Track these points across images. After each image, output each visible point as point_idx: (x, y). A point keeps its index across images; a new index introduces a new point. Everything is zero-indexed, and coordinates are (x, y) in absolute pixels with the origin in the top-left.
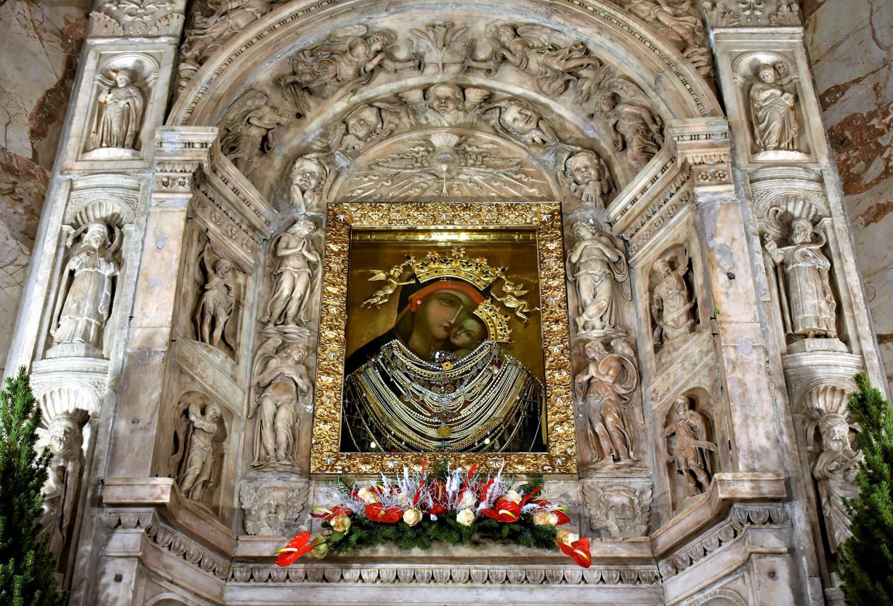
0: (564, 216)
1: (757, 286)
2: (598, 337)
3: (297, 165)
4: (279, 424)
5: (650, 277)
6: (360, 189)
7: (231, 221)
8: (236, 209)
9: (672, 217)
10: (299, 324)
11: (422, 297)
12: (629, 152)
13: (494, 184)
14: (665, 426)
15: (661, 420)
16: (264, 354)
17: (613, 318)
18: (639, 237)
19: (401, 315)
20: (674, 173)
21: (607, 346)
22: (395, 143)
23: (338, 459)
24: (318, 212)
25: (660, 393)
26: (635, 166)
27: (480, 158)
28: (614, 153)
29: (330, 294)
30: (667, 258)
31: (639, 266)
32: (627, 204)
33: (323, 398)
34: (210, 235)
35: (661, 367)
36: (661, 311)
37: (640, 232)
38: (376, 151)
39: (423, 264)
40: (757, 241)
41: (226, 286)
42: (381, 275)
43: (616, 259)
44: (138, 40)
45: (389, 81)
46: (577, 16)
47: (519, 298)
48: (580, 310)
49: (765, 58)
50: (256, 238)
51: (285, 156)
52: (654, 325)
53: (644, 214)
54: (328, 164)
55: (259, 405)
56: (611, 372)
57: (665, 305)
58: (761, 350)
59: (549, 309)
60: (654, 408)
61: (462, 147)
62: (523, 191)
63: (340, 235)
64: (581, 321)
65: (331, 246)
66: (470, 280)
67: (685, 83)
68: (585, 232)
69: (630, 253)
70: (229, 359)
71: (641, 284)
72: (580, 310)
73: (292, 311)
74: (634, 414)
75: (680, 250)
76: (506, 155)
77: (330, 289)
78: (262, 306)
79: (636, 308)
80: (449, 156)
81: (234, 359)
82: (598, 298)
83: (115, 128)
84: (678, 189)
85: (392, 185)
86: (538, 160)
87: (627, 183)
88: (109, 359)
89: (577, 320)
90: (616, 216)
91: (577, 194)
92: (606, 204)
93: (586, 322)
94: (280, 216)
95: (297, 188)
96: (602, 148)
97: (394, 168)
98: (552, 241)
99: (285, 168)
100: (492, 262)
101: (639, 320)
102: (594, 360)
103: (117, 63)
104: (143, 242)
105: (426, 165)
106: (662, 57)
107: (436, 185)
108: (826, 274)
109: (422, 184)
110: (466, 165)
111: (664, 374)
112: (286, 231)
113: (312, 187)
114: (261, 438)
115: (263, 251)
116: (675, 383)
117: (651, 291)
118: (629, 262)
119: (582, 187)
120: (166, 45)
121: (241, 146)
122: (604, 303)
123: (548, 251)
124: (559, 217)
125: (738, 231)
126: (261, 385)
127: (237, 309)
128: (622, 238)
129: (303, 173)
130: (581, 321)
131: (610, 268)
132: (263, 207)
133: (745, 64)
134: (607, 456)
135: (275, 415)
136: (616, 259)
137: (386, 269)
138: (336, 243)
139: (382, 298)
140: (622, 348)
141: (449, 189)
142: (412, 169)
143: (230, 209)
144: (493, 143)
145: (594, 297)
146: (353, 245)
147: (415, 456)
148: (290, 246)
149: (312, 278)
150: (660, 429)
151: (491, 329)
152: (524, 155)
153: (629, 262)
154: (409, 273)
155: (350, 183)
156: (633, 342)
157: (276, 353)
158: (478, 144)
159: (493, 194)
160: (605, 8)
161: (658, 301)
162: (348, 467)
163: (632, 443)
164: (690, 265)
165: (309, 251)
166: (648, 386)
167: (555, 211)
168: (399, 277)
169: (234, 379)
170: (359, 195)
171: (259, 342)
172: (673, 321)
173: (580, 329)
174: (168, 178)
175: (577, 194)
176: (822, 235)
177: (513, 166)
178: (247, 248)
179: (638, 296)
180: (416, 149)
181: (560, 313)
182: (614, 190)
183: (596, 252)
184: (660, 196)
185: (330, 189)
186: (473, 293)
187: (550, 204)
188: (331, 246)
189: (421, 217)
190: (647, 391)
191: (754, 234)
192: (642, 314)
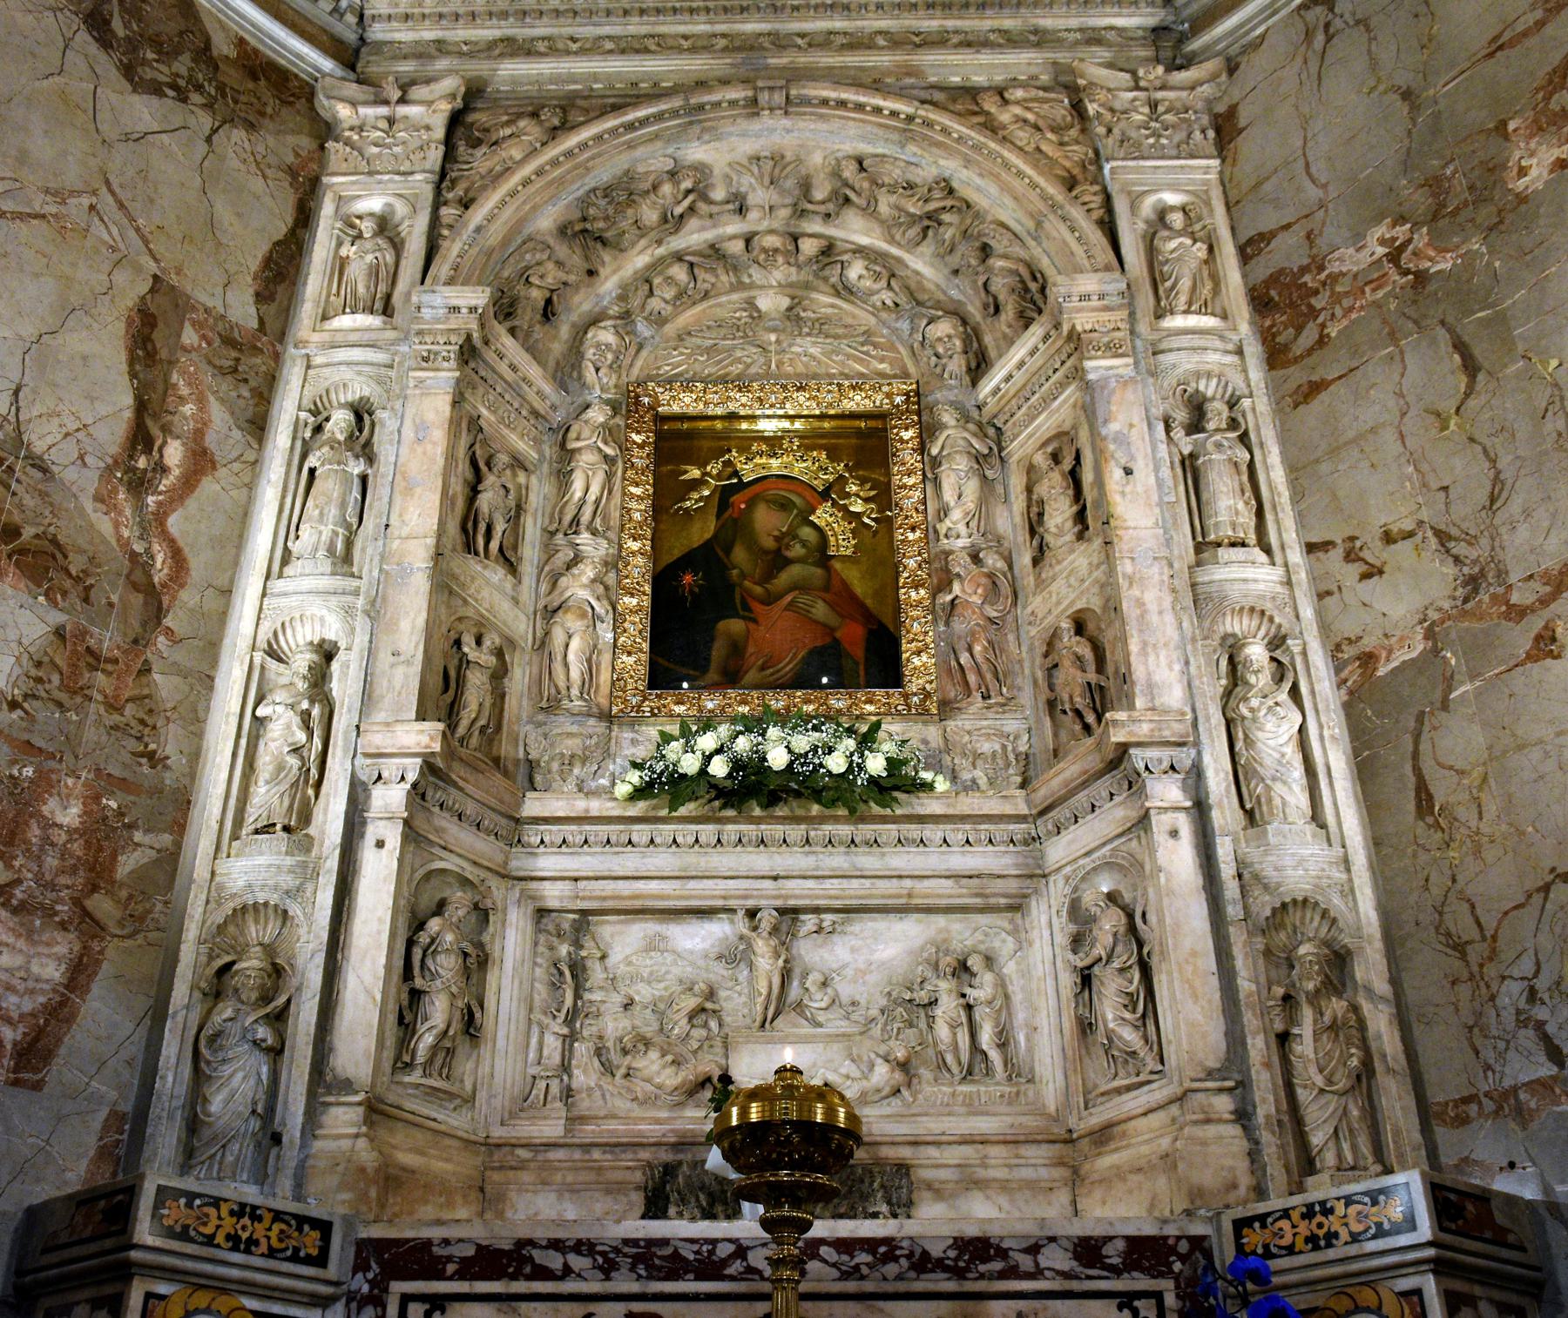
1: (1160, 483)
3: (590, 335)
4: (571, 657)
5: (1028, 473)
10: (594, 533)
12: (1003, 317)
14: (1046, 655)
20: (1060, 343)
21: (976, 558)
23: (645, 699)
29: (632, 496)
30: (1050, 449)
33: (626, 625)
35: (1041, 584)
36: (1041, 515)
40: (1160, 427)
42: (695, 473)
43: (986, 451)
47: (866, 500)
49: (1172, 198)
51: (574, 325)
52: (1033, 532)
55: (547, 633)
57: (1047, 507)
60: (1033, 633)
61: (795, 311)
65: (633, 436)
66: (805, 478)
68: (948, 418)
71: (1017, 482)
75: (1065, 439)
76: (849, 321)
77: (633, 490)
82: (964, 499)
83: (361, 290)
84: (1063, 363)
87: (1000, 356)
91: (938, 370)
94: (569, 399)
98: (907, 429)
100: (833, 456)
101: (1014, 526)
102: (958, 575)
104: (399, 432)
106: (1045, 197)
107: (762, 360)
108: (1244, 468)
116: (1058, 603)
117: (1029, 490)
120: (421, 183)
121: (519, 311)
122: (971, 506)
123: (902, 441)
125: (1137, 417)
127: (518, 516)
128: (994, 425)
129: (598, 346)
132: (547, 388)
136: (986, 451)
137: (702, 465)
138: (638, 433)
139: (697, 501)
140: (993, 561)
144: (833, 306)
149: (609, 476)
150: (1038, 661)
152: (873, 321)
154: (730, 469)
160: (973, 134)
165: (606, 443)
166: (1024, 607)
169: (516, 601)
174: (429, 351)
175: (938, 370)
176: (1241, 420)
179: (1013, 498)
183: (962, 442)
186: (808, 494)
189: (744, 400)
190: (1023, 613)
192: (1018, 519)
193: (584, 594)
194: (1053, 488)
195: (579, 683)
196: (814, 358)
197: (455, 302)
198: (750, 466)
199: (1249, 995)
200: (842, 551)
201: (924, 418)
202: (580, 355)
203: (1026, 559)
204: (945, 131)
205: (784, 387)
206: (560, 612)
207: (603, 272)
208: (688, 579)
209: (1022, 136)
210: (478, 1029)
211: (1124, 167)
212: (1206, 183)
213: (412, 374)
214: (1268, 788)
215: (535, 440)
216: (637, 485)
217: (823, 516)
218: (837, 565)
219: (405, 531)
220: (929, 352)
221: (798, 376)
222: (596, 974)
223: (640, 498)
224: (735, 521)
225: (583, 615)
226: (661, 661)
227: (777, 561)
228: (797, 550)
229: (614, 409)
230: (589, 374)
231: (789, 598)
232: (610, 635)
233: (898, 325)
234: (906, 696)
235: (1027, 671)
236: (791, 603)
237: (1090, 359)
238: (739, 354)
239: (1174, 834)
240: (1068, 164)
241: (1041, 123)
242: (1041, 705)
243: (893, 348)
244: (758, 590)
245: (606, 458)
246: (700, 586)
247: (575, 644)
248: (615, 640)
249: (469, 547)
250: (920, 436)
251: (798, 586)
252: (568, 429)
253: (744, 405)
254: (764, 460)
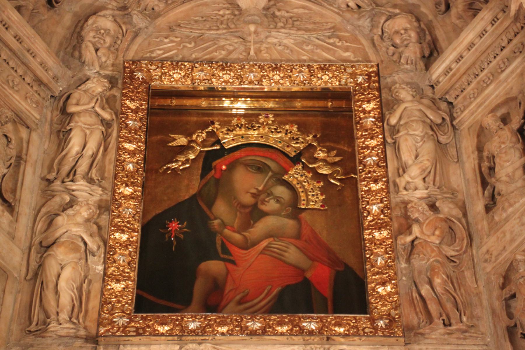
0: (382, 79)
2: (421, 199)
3: (90, 21)
4: (62, 284)
5: (478, 136)
6: (160, 50)
7: (13, 72)
8: (19, 58)
9: (502, 71)
10: (91, 181)
11: (227, 163)
12: (453, 11)
13: (305, 47)
14: (503, 287)
16: (49, 212)
17: (438, 178)
18: (465, 98)
19: (204, 181)
20: (507, 23)
21: (433, 207)
22: (198, 6)
23: (131, 320)
24: (113, 71)
25: (495, 253)
26: (460, 26)
27: (290, 21)
28: (436, 16)
29: (125, 150)
30: (499, 114)
31: (466, 125)
32: (452, 62)
33: (116, 257)
35: (494, 227)
36: (492, 169)
37: (465, 93)
39: (229, 130)
41: (6, 136)
42: (182, 140)
43: (439, 121)
47: (333, 164)
48: (401, 171)
50: (42, 94)
51: (75, 14)
52: (484, 184)
53: (470, 72)
54: (124, 23)
55: (41, 266)
56: (437, 233)
57: (497, 160)
59: (367, 169)
60: (488, 270)
61: (271, 11)
62: (337, 55)
63: (139, 93)
64: (402, 182)
65: (128, 102)
66: (279, 146)
68: (405, 94)
69: (455, 115)
70: (7, 214)
72: (401, 171)
73: (83, 167)
74: (464, 277)
75: (513, 104)
76: (318, 19)
77: (127, 146)
78: (47, 163)
79: (463, 169)
80: (256, 17)
81: (12, 215)
82: (420, 159)
84: (510, 41)
85: (195, 47)
86: (352, 25)
87: (450, 42)
89: (398, 180)
90: (439, 76)
91: (395, 58)
92: (427, 67)
93: (408, 183)
94: (70, 73)
95: (90, 45)
96: (422, 12)
97: (198, 29)
98: (369, 102)
99: (76, 26)
100: (304, 129)
101: (467, 181)
102: (417, 221)
105: (233, 26)
107: (242, 48)
109: (228, 47)
110: (275, 27)
111: (498, 233)
112: (77, 88)
113: (107, 45)
114: (41, 300)
115: (50, 109)
116: (513, 240)
117: (480, 149)
118: (454, 123)
119: (401, 49)
122: (427, 164)
123: (364, 111)
124: (376, 78)
126: (44, 244)
127: (18, 165)
128: (446, 101)
129: (98, 30)
130: (402, 182)
131: (432, 130)
132: (51, 62)
134: (436, 320)
135: (59, 276)
136: (439, 121)
137: (187, 134)
138: (133, 100)
139: (184, 163)
141: (258, 51)
142: (218, 30)
143: (11, 59)
144: (304, 7)
145: (416, 157)
146: (151, 111)
147: (219, 317)
148: (82, 102)
149: (106, 137)
150: (496, 292)
151: (302, 194)
152: (338, 19)
153: (454, 123)
154: (213, 140)
155: (149, 44)
156: (460, 204)
157: (63, 211)
158: (288, 8)
159: (304, 58)
161: (488, 158)
162: (143, 328)
163: (465, 307)
165: (103, 108)
166: (479, 248)
167: (372, 72)
168: (202, 142)
169: (12, 237)
170: (159, 55)
171: (44, 201)
172: (508, 176)
173: (401, 189)
175: (395, 58)
177: (325, 30)
178: (32, 102)
179: (465, 157)
180: (221, 12)
181: (380, 172)
182: (435, 54)
183: (417, 113)
184: (489, 51)
185: (127, 49)
186: (282, 159)
187: (367, 66)
188: (128, 102)
189: (226, 77)
190: (478, 253)
192: (470, 175)
193: (78, 231)
195: (69, 308)
196: (286, 47)
198: (230, 136)
200: (312, 205)
201: (384, 95)
202: (80, 39)
203: (480, 207)
205: (261, 68)
206: (54, 247)
208: (174, 226)
215: (37, 103)
216: (130, 142)
220: (388, 43)
221: (273, 61)
223: (132, 153)
224: (217, 182)
225: (76, 249)
226: (145, 295)
228: (271, 205)
229: (111, 82)
230: (89, 54)
231: (264, 244)
232: (100, 268)
233: (360, 23)
234: (373, 321)
235: (485, 303)
236: (266, 249)
238: (222, 43)
242: (500, 332)
243: (356, 40)
244: (237, 237)
245: (103, 121)
246: (184, 233)
247: (66, 273)
248: (105, 269)
250: (381, 107)
252: (68, 97)
253: (226, 82)
254: (243, 132)
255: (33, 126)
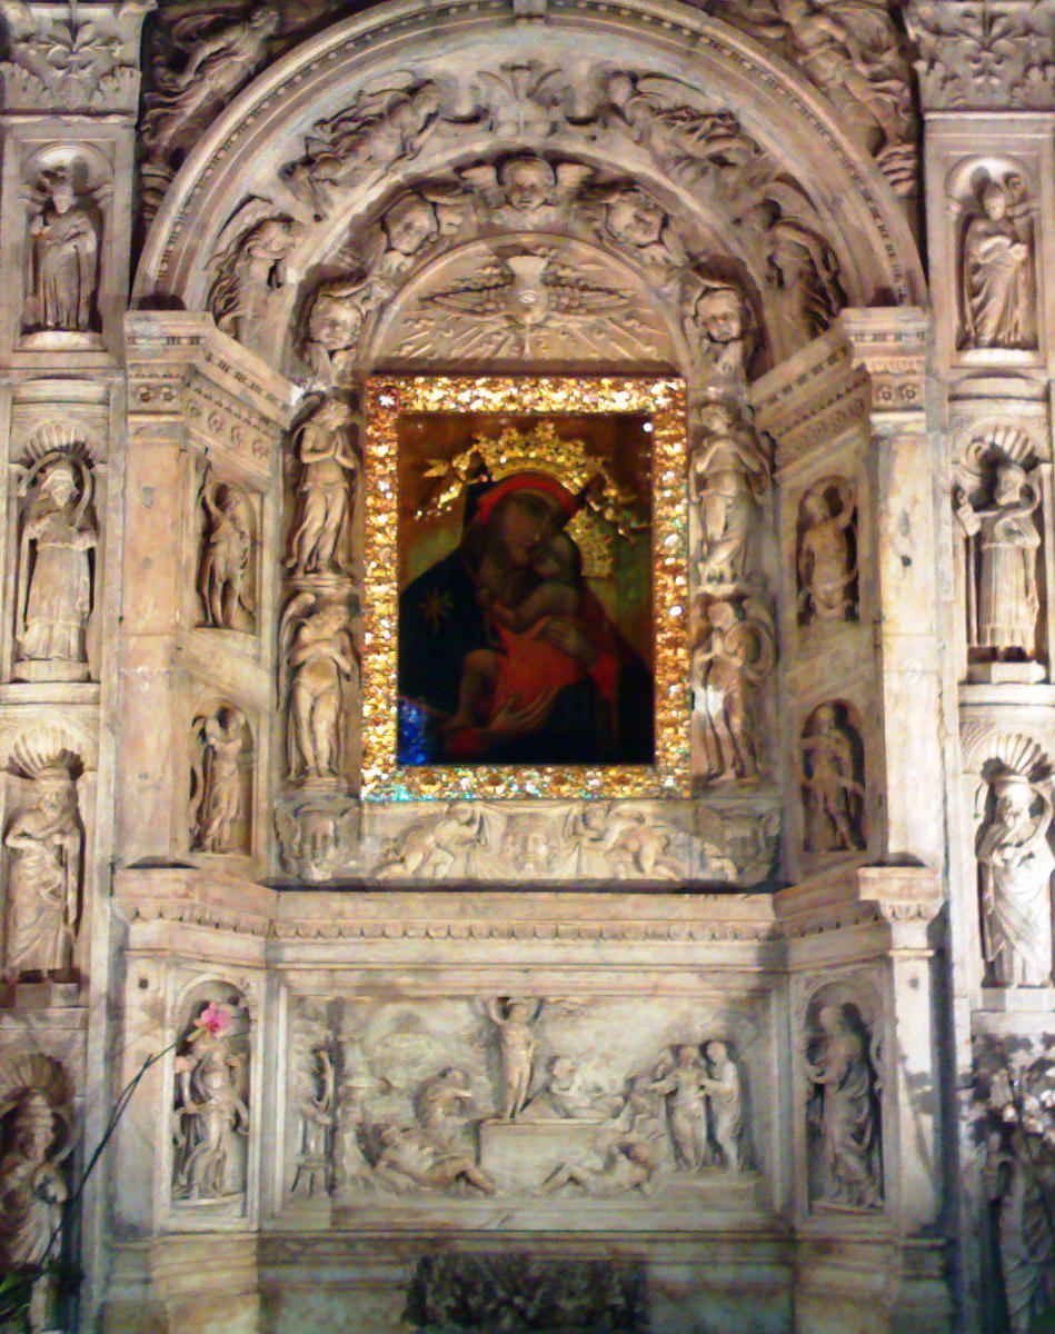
1: (939, 574)
6: (410, 344)
15: (800, 727)
34: (211, 457)
35: (806, 653)
38: (432, 275)
40: (947, 503)
44: (75, 119)
45: (445, 149)
46: (726, 77)
49: (996, 168)
58: (934, 678)
67: (876, 215)
71: (789, 516)
73: (326, 552)
83: (63, 295)
88: (98, 682)
90: (762, 402)
103: (50, 158)
104: (123, 494)
106: (848, 165)
108: (1032, 556)
120: (118, 131)
121: (241, 297)
125: (923, 490)
133: (963, 182)
140: (758, 611)
144: (594, 261)
152: (639, 284)
160: (768, 65)
164: (855, 517)
169: (257, 659)
174: (148, 386)
176: (1037, 490)
191: (944, 491)
194: (823, 540)
197: (174, 331)
199: (971, 1164)
204: (737, 58)
207: (332, 214)
209: (829, 67)
210: (247, 1129)
211: (943, 121)
212: (1036, 145)
213: (132, 419)
214: (1012, 947)
217: (578, 528)
218: (593, 585)
219: (141, 626)
222: (354, 1058)
227: (529, 578)
237: (879, 410)
239: (914, 983)
240: (875, 110)
241: (852, 47)
244: (509, 613)
249: (211, 621)
251: (553, 610)
255: (264, 488)
